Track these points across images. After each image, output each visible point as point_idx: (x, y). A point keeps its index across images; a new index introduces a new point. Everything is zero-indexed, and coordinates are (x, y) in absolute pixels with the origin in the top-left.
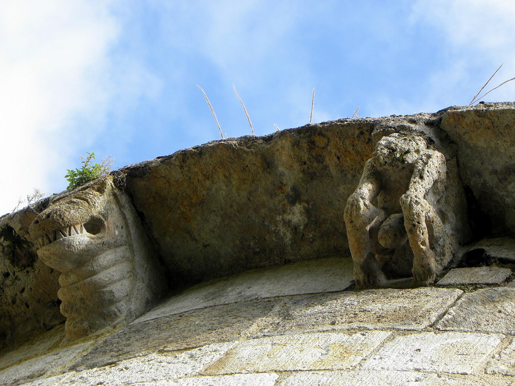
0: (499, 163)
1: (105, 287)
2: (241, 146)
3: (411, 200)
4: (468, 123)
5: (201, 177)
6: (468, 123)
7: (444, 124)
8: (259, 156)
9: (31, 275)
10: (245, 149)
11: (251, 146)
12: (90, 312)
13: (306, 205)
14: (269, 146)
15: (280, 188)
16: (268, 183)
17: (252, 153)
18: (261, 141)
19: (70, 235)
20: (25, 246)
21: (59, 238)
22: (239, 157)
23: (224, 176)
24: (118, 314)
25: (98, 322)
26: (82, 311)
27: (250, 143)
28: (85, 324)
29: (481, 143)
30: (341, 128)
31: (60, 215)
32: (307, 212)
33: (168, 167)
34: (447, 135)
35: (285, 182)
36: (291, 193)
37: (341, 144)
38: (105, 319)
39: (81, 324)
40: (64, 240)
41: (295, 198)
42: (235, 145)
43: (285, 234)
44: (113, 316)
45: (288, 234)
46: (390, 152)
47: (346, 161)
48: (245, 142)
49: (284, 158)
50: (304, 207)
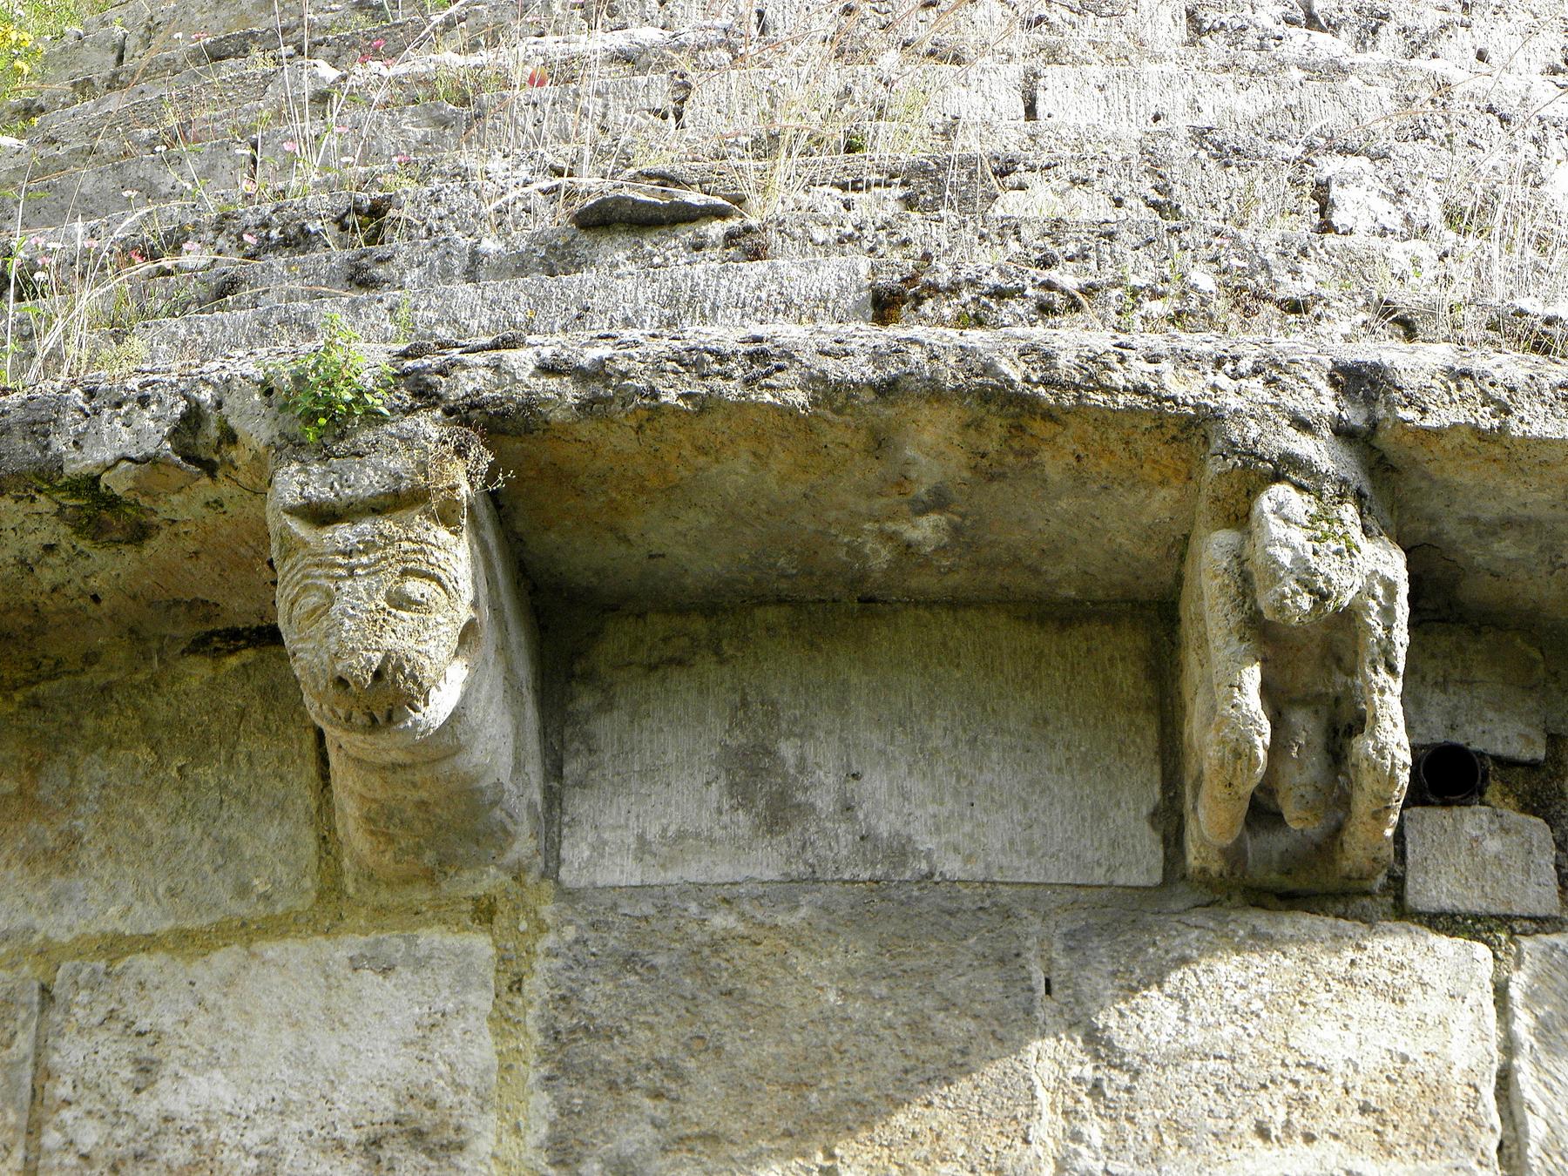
0: (1491, 510)
1: (477, 780)
2: (818, 406)
3: (1393, 765)
4: (1449, 447)
5: (687, 451)
6: (1449, 447)
7: (1384, 440)
8: (863, 432)
9: (129, 557)
10: (830, 415)
11: (844, 406)
12: (440, 828)
13: (957, 519)
14: (890, 412)
15: (900, 485)
16: (871, 476)
17: (847, 427)
18: (868, 396)
19: (426, 704)
20: (129, 511)
21: (403, 720)
22: (810, 429)
23: (754, 454)
24: (511, 827)
25: (461, 851)
26: (418, 825)
27: (840, 400)
28: (429, 857)
29: (1467, 478)
30: (1110, 415)
31: (415, 678)
32: (956, 530)
33: (601, 427)
34: (1383, 457)
35: (913, 475)
36: (925, 498)
37: (1097, 437)
38: (478, 843)
39: (418, 856)
40: (416, 723)
41: (938, 501)
42: (803, 407)
43: (876, 552)
44: (500, 834)
45: (884, 552)
46: (1315, 602)
47: (1098, 465)
48: (825, 394)
49: (927, 437)
50: (949, 522)
